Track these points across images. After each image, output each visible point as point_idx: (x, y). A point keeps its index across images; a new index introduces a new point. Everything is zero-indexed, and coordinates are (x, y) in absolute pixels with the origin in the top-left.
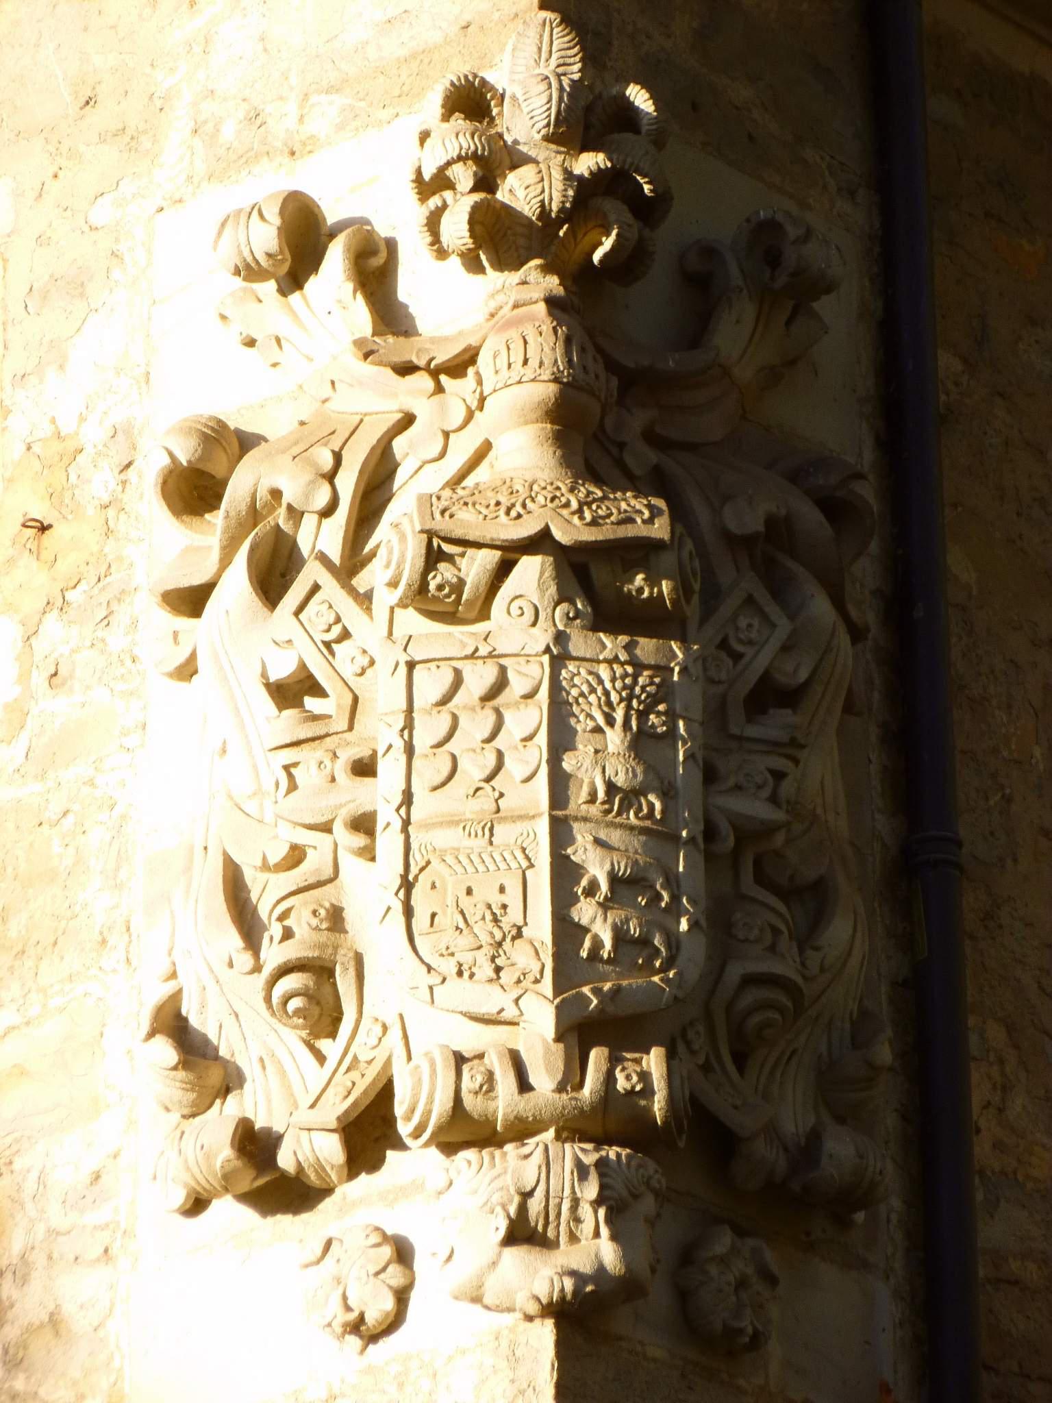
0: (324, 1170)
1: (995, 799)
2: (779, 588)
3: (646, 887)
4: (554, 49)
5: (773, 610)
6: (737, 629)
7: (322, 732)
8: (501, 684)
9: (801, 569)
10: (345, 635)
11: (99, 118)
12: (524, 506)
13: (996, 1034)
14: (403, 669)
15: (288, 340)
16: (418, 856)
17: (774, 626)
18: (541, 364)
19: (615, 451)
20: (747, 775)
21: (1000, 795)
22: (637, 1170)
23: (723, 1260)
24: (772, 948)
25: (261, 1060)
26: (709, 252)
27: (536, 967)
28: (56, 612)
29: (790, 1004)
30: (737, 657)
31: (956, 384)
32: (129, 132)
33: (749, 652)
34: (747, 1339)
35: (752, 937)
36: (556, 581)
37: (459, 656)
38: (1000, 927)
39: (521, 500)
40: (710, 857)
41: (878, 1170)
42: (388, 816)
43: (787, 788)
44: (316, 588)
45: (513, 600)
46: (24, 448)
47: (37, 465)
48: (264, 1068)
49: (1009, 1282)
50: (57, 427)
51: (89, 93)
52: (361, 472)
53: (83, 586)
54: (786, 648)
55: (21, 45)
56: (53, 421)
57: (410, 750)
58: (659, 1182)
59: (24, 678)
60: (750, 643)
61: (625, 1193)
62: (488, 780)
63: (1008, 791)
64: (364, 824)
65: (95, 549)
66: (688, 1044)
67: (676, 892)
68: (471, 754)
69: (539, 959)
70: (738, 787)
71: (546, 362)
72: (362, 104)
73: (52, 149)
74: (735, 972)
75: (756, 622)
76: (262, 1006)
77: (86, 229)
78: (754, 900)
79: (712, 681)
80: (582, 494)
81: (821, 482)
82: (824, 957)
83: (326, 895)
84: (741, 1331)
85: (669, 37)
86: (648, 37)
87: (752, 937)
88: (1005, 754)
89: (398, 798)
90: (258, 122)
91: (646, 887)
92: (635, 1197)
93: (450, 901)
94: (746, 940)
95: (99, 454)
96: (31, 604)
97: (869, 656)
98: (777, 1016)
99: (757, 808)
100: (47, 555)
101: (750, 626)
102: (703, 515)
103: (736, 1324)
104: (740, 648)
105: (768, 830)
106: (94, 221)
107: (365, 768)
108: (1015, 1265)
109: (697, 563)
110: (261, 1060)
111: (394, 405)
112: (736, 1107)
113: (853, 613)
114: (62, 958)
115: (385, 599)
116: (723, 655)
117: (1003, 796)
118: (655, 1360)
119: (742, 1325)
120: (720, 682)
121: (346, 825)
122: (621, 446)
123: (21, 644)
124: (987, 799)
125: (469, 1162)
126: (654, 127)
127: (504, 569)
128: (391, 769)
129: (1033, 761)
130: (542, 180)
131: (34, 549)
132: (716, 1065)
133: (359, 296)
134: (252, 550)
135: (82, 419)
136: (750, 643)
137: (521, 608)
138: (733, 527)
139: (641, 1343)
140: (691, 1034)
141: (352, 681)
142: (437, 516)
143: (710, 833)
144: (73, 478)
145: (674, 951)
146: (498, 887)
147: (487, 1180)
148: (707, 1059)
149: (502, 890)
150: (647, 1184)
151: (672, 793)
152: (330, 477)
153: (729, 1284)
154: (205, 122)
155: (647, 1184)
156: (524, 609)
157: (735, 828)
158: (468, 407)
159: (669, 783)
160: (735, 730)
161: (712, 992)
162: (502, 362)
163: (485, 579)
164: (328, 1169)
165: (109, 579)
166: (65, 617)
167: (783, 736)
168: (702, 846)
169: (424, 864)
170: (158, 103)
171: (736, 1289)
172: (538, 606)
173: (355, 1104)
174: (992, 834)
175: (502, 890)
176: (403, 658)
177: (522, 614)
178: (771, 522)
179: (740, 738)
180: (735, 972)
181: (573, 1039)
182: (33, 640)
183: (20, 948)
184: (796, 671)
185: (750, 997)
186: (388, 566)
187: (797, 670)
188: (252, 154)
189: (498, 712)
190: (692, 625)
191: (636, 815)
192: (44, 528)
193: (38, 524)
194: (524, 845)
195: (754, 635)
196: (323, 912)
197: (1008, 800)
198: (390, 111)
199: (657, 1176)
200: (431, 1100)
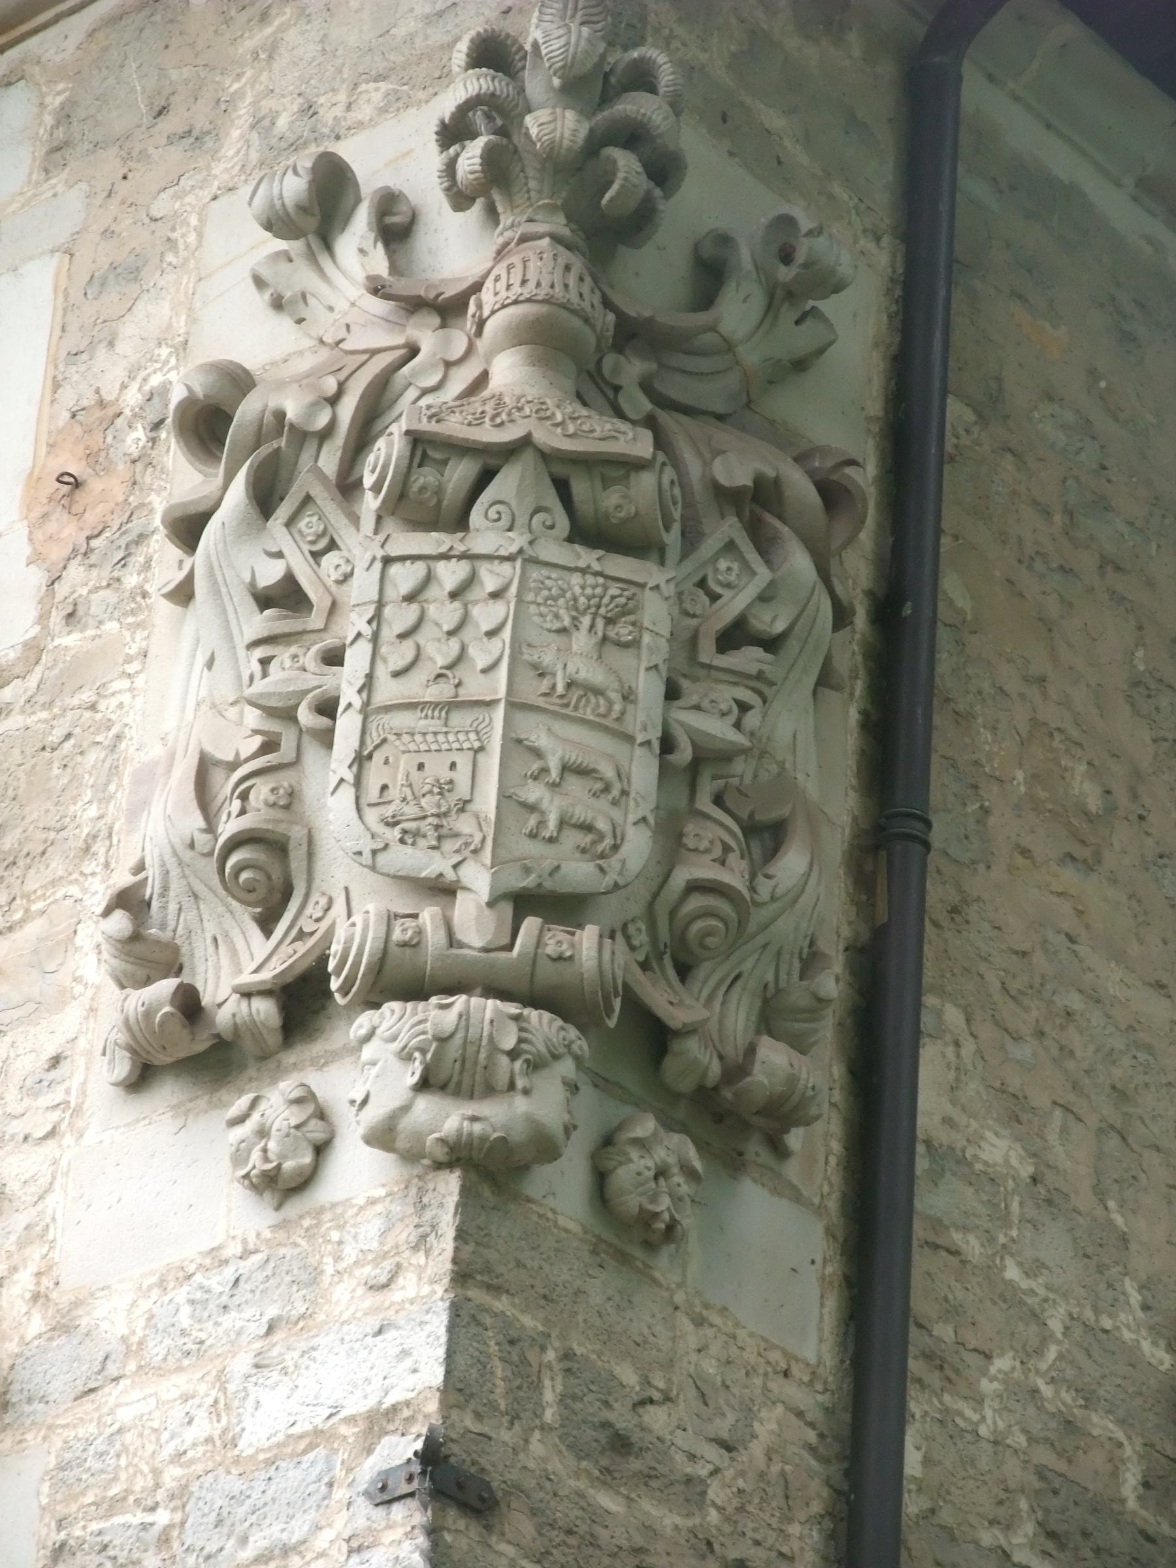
0: (261, 1034)
1: (973, 807)
2: (765, 544)
3: (597, 778)
4: (580, 6)
5: (752, 556)
6: (716, 570)
7: (299, 629)
8: (471, 581)
9: (787, 529)
10: (332, 545)
11: (171, 124)
12: (509, 414)
13: (953, 1016)
14: (378, 565)
15: (313, 295)
16: (374, 734)
17: (754, 573)
18: (538, 285)
19: (611, 394)
20: (713, 701)
21: (978, 805)
22: (558, 1031)
23: (640, 1143)
24: (723, 863)
25: (215, 940)
26: (724, 240)
27: (478, 838)
28: (79, 558)
29: (734, 915)
30: (714, 597)
31: (967, 431)
32: (195, 134)
33: (727, 594)
34: (662, 1226)
35: (702, 848)
36: (846, 1465)
37: (434, 553)
38: (968, 922)
39: (507, 409)
40: (665, 771)
41: (810, 1085)
42: (349, 695)
43: (752, 720)
44: (308, 500)
45: (491, 506)
46: (68, 415)
47: (78, 430)
48: (217, 947)
49: (948, 1251)
50: (100, 396)
51: (163, 103)
52: (362, 397)
53: (107, 534)
54: (764, 598)
55: (107, 68)
56: (98, 391)
57: (375, 638)
58: (581, 1048)
59: (43, 619)
60: (728, 586)
61: (543, 1050)
62: (450, 667)
63: (987, 804)
64: (328, 708)
65: (121, 498)
66: (628, 939)
67: (626, 787)
68: (436, 644)
69: (481, 830)
70: (697, 708)
71: (543, 283)
72: (405, 87)
73: (125, 155)
74: (681, 877)
75: (736, 566)
76: (216, 880)
77: (147, 220)
78: (707, 817)
79: (686, 613)
80: (569, 409)
81: (817, 464)
82: (775, 887)
83: (285, 779)
84: (656, 1215)
85: (706, 51)
86: (684, 45)
87: (702, 848)
88: (987, 769)
89: (361, 681)
90: (310, 113)
91: (597, 778)
92: (556, 1057)
93: (400, 777)
94: (696, 850)
95: (135, 415)
96: (57, 553)
97: (856, 648)
98: (720, 925)
99: (718, 729)
100: (77, 508)
101: (729, 569)
102: (694, 469)
103: (651, 1207)
104: (718, 590)
105: (725, 756)
106: (156, 213)
107: (334, 658)
108: (957, 1237)
109: (677, 491)
110: (215, 940)
111: (400, 340)
112: (671, 1003)
113: (839, 589)
114: (48, 866)
115: (370, 503)
116: (701, 592)
117: (982, 807)
118: (567, 1231)
119: (658, 1209)
120: (694, 616)
121: (310, 708)
122: (617, 389)
123: (45, 588)
124: (965, 805)
125: (393, 1012)
126: (671, 89)
127: (486, 477)
128: (357, 659)
129: (1015, 783)
130: (555, 120)
131: (66, 505)
132: (655, 966)
133: (380, 245)
134: (251, 465)
135: (124, 387)
136: (728, 586)
137: (499, 513)
138: (724, 480)
139: (554, 1211)
140: (631, 929)
141: (334, 588)
142: (425, 420)
143: (667, 745)
144: (109, 439)
145: (619, 842)
146: (449, 764)
147: (407, 1027)
148: (647, 958)
149: (453, 766)
150: (568, 1047)
151: (632, 698)
152: (334, 401)
153: (648, 1169)
154: (263, 118)
155: (568, 1046)
156: (503, 516)
157: (695, 745)
158: (469, 336)
159: (630, 687)
160: (704, 658)
161: (656, 896)
162: (501, 285)
163: (466, 486)
164: (264, 1032)
165: (130, 525)
166: (87, 562)
167: (753, 669)
168: (658, 751)
169: (377, 742)
170: (223, 107)
171: (656, 1178)
172: (516, 513)
173: (291, 966)
174: (967, 837)
175: (453, 766)
176: (380, 553)
177: (499, 520)
178: (759, 480)
179: (709, 667)
180: (681, 877)
181: (507, 909)
182: (56, 585)
183: (11, 859)
184: (774, 619)
185: (696, 902)
186: (373, 471)
187: (774, 621)
188: (301, 141)
189: (466, 606)
190: (673, 553)
191: (593, 710)
192: (77, 484)
193: (72, 480)
194: (479, 728)
195: (732, 578)
196: (282, 791)
197: (986, 811)
198: (431, 90)
199: (579, 1042)
200: (360, 954)
